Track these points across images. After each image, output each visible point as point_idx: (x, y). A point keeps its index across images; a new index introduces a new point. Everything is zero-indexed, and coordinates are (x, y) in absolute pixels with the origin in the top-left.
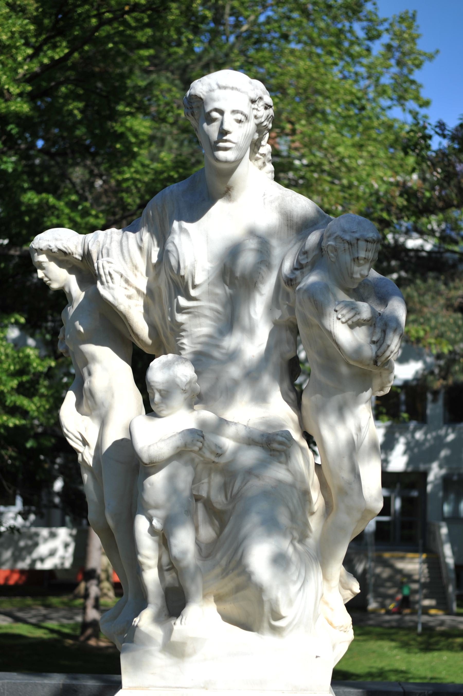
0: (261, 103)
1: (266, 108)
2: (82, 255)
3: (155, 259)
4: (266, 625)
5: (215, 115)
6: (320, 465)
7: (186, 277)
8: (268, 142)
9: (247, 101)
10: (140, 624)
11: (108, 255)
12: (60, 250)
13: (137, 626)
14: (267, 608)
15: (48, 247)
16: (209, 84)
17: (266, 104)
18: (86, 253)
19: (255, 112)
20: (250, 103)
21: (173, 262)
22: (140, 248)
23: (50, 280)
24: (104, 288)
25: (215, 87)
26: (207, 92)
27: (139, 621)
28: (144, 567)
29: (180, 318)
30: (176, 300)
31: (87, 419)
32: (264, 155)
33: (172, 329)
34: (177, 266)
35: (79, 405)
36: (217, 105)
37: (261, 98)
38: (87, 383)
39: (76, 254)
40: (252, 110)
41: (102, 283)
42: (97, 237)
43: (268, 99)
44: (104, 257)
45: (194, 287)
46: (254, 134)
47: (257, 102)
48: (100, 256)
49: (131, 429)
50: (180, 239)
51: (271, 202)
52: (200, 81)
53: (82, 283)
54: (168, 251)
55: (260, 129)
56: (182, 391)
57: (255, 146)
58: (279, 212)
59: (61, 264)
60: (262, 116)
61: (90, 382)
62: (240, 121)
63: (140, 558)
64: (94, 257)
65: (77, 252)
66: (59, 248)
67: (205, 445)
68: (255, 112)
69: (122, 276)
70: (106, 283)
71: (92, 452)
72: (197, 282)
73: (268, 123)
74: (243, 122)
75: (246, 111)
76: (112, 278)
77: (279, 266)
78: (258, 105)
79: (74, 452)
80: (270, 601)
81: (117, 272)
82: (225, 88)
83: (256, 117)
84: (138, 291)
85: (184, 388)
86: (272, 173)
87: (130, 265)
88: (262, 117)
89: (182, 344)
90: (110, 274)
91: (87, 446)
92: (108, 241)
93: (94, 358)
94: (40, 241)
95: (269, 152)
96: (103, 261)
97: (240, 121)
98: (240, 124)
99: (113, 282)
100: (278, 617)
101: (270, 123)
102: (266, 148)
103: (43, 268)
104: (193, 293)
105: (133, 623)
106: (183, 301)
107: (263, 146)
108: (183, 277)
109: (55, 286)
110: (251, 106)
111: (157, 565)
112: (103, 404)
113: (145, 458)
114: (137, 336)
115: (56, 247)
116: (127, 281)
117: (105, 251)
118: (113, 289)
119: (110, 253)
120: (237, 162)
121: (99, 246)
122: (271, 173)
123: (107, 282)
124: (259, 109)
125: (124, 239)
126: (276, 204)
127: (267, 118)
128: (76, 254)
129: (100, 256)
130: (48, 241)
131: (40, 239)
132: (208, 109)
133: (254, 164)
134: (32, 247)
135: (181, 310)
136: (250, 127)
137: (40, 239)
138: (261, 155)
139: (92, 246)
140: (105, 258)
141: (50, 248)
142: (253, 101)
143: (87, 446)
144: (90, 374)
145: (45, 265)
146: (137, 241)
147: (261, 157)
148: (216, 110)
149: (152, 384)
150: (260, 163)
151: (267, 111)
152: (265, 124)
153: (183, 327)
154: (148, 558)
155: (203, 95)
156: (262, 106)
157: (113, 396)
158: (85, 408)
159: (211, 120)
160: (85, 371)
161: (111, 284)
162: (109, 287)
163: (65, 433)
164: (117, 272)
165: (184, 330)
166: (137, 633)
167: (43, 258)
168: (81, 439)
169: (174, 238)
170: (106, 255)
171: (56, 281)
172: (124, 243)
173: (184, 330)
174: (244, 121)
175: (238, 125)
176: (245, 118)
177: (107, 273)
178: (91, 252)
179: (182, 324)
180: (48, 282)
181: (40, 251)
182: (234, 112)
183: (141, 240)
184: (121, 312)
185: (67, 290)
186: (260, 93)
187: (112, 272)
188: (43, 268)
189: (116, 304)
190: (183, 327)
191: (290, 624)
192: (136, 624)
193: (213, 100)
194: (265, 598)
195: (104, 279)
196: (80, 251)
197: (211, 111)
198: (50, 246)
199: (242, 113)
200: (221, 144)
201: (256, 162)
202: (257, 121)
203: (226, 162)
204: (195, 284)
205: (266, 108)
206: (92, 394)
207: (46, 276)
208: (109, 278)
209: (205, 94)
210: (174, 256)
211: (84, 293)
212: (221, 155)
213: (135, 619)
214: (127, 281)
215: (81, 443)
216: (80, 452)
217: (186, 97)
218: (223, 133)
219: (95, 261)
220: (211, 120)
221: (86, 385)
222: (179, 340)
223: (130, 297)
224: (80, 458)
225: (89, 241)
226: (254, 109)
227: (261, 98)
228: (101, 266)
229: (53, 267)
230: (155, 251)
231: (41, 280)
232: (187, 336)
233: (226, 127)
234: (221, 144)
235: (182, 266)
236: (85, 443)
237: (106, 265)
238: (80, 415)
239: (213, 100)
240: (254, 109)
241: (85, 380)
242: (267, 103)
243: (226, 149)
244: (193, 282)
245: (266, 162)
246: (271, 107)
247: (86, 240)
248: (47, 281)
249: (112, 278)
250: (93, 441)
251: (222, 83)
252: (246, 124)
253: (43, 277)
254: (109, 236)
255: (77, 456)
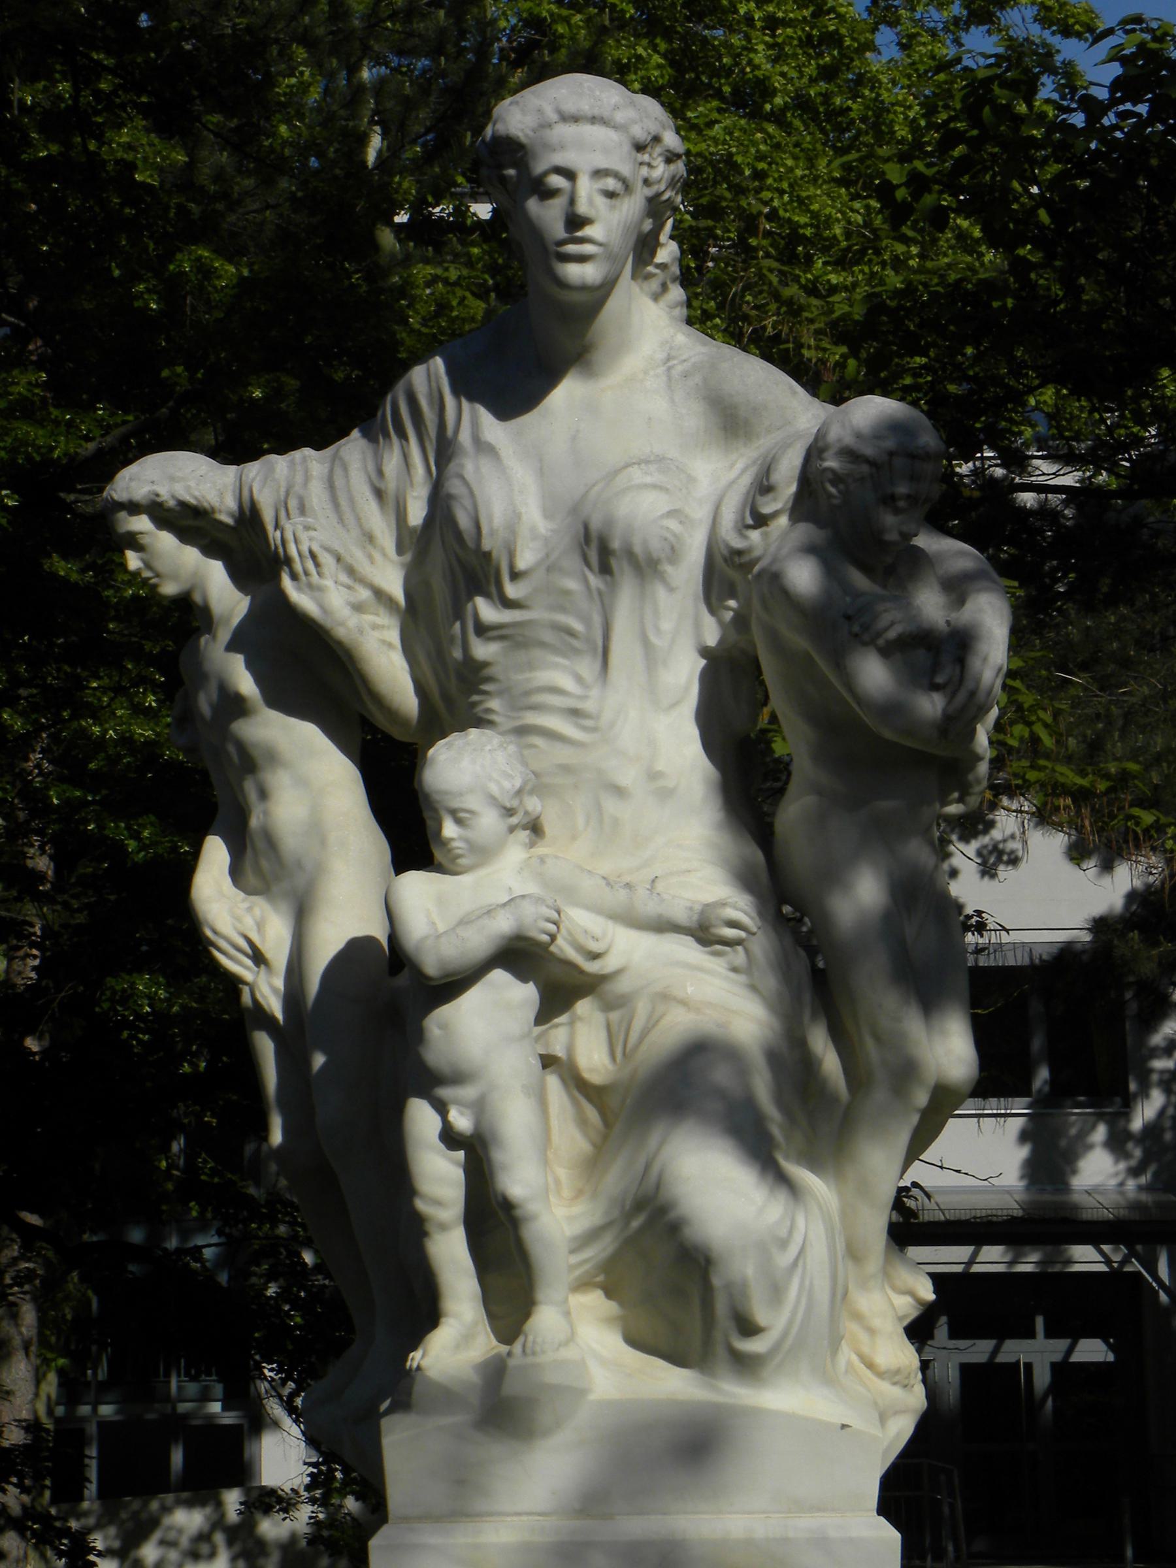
0: (658, 150)
1: (668, 161)
2: (237, 514)
3: (416, 514)
4: (720, 1351)
5: (556, 181)
6: (823, 971)
7: (494, 554)
8: (672, 237)
9: (627, 147)
10: (424, 1364)
11: (302, 510)
12: (183, 504)
13: (419, 1368)
14: (721, 1308)
15: (153, 497)
16: (540, 111)
17: (668, 151)
18: (247, 512)
19: (644, 171)
20: (634, 153)
21: (463, 520)
22: (379, 494)
23: (158, 575)
24: (299, 589)
25: (554, 117)
26: (534, 131)
27: (423, 1356)
28: (429, 1227)
29: (482, 650)
30: (469, 606)
31: (261, 905)
32: (663, 266)
33: (462, 678)
34: (473, 531)
35: (236, 872)
36: (559, 159)
37: (657, 139)
38: (258, 818)
39: (220, 511)
40: (637, 166)
41: (294, 577)
42: (271, 469)
43: (671, 140)
44: (292, 517)
45: (515, 576)
46: (641, 222)
47: (649, 149)
48: (283, 514)
49: (391, 903)
50: (477, 469)
51: (686, 375)
52: (517, 103)
53: (240, 576)
54: (450, 497)
55: (656, 208)
56: (503, 811)
57: (643, 246)
58: (704, 398)
59: (186, 535)
60: (661, 179)
61: (266, 813)
62: (610, 195)
63: (420, 1205)
64: (268, 517)
65: (223, 508)
66: (181, 498)
67: (563, 930)
68: (644, 171)
69: (339, 559)
70: (303, 578)
71: (279, 983)
72: (522, 564)
73: (673, 194)
74: (618, 195)
75: (625, 170)
76: (317, 565)
77: (710, 521)
78: (650, 155)
79: (232, 983)
80: (728, 1286)
81: (327, 549)
82: (576, 119)
83: (646, 182)
84: (379, 594)
85: (508, 805)
86: (682, 306)
87: (355, 532)
88: (659, 181)
89: (489, 711)
90: (313, 556)
91: (263, 967)
92: (299, 478)
93: (273, 757)
94: (133, 484)
95: (674, 259)
96: (294, 524)
97: (610, 195)
98: (614, 201)
99: (319, 574)
100: (749, 1329)
101: (677, 194)
102: (668, 251)
103: (139, 548)
104: (512, 590)
105: (408, 1364)
106: (487, 611)
107: (663, 245)
108: (487, 556)
109: (169, 589)
110: (635, 159)
111: (462, 1220)
112: (299, 865)
113: (431, 967)
114: (377, 698)
115: (173, 497)
116: (351, 571)
117: (293, 504)
118: (320, 589)
119: (307, 506)
120: (606, 288)
121: (278, 491)
122: (679, 308)
123: (306, 573)
124: (654, 163)
125: (338, 472)
126: (698, 379)
127: (672, 183)
128: (220, 511)
129: (283, 514)
130: (153, 482)
131: (131, 479)
132: (539, 168)
133: (641, 288)
134: (112, 498)
135: (482, 630)
136: (632, 207)
137: (131, 479)
138: (658, 266)
139: (260, 491)
140: (298, 519)
141: (159, 500)
142: (640, 147)
143: (263, 967)
144: (263, 794)
145: (144, 540)
146: (369, 478)
147: (657, 271)
148: (559, 170)
149: (436, 797)
150: (654, 285)
151: (672, 167)
152: (666, 196)
153: (487, 672)
154: (438, 1203)
155: (526, 136)
156: (660, 155)
157: (323, 842)
158: (251, 879)
159: (548, 194)
160: (249, 786)
161: (315, 578)
162: (310, 586)
163: (207, 938)
164: (327, 549)
165: (489, 679)
166: (417, 1388)
167: (142, 524)
168: (249, 951)
169: (462, 466)
170: (297, 512)
171: (175, 577)
172: (339, 482)
173: (489, 679)
174: (622, 192)
175: (608, 201)
176: (623, 188)
177: (307, 554)
178: (258, 507)
179: (485, 664)
180: (153, 581)
181: (134, 508)
182: (598, 174)
183: (380, 473)
184: (339, 643)
185: (197, 598)
186: (654, 128)
187: (316, 548)
188: (139, 548)
189: (326, 622)
190: (487, 672)
191: (776, 1348)
192: (415, 1365)
193: (550, 148)
194: (716, 1281)
195: (298, 567)
196: (231, 503)
197: (546, 173)
198: (157, 495)
199: (616, 175)
200: (571, 248)
201: (645, 285)
202: (649, 192)
203: (584, 288)
204: (516, 570)
205: (668, 161)
206: (270, 840)
207: (148, 566)
208: (310, 565)
209: (531, 134)
210: (466, 509)
211: (248, 598)
212: (574, 272)
213: (411, 1355)
214: (351, 571)
215: (249, 962)
216: (246, 983)
217: (483, 141)
218: (575, 222)
219: (270, 528)
220: (548, 194)
221: (254, 822)
222: (480, 702)
223: (358, 608)
224: (246, 998)
225: (253, 479)
226: (641, 164)
227: (657, 139)
228: (289, 536)
229: (165, 541)
230: (415, 498)
231: (136, 574)
232: (500, 693)
233: (582, 208)
234: (571, 248)
235: (485, 530)
236: (258, 958)
237: (303, 536)
238: (242, 895)
239: (550, 148)
240: (641, 164)
241: (250, 812)
242: (671, 148)
243: (582, 259)
244: (512, 566)
245: (668, 283)
246: (678, 156)
247: (244, 478)
248: (149, 579)
249: (317, 565)
250: (279, 950)
251: (570, 107)
252: (626, 200)
253: (140, 569)
254: (299, 468)
255: (237, 994)
